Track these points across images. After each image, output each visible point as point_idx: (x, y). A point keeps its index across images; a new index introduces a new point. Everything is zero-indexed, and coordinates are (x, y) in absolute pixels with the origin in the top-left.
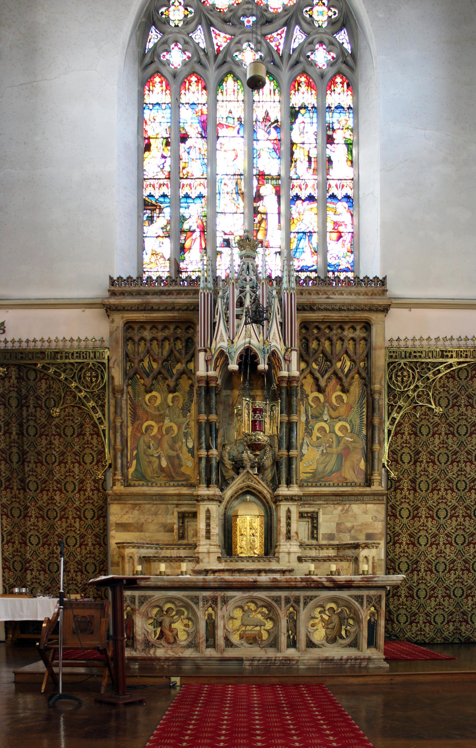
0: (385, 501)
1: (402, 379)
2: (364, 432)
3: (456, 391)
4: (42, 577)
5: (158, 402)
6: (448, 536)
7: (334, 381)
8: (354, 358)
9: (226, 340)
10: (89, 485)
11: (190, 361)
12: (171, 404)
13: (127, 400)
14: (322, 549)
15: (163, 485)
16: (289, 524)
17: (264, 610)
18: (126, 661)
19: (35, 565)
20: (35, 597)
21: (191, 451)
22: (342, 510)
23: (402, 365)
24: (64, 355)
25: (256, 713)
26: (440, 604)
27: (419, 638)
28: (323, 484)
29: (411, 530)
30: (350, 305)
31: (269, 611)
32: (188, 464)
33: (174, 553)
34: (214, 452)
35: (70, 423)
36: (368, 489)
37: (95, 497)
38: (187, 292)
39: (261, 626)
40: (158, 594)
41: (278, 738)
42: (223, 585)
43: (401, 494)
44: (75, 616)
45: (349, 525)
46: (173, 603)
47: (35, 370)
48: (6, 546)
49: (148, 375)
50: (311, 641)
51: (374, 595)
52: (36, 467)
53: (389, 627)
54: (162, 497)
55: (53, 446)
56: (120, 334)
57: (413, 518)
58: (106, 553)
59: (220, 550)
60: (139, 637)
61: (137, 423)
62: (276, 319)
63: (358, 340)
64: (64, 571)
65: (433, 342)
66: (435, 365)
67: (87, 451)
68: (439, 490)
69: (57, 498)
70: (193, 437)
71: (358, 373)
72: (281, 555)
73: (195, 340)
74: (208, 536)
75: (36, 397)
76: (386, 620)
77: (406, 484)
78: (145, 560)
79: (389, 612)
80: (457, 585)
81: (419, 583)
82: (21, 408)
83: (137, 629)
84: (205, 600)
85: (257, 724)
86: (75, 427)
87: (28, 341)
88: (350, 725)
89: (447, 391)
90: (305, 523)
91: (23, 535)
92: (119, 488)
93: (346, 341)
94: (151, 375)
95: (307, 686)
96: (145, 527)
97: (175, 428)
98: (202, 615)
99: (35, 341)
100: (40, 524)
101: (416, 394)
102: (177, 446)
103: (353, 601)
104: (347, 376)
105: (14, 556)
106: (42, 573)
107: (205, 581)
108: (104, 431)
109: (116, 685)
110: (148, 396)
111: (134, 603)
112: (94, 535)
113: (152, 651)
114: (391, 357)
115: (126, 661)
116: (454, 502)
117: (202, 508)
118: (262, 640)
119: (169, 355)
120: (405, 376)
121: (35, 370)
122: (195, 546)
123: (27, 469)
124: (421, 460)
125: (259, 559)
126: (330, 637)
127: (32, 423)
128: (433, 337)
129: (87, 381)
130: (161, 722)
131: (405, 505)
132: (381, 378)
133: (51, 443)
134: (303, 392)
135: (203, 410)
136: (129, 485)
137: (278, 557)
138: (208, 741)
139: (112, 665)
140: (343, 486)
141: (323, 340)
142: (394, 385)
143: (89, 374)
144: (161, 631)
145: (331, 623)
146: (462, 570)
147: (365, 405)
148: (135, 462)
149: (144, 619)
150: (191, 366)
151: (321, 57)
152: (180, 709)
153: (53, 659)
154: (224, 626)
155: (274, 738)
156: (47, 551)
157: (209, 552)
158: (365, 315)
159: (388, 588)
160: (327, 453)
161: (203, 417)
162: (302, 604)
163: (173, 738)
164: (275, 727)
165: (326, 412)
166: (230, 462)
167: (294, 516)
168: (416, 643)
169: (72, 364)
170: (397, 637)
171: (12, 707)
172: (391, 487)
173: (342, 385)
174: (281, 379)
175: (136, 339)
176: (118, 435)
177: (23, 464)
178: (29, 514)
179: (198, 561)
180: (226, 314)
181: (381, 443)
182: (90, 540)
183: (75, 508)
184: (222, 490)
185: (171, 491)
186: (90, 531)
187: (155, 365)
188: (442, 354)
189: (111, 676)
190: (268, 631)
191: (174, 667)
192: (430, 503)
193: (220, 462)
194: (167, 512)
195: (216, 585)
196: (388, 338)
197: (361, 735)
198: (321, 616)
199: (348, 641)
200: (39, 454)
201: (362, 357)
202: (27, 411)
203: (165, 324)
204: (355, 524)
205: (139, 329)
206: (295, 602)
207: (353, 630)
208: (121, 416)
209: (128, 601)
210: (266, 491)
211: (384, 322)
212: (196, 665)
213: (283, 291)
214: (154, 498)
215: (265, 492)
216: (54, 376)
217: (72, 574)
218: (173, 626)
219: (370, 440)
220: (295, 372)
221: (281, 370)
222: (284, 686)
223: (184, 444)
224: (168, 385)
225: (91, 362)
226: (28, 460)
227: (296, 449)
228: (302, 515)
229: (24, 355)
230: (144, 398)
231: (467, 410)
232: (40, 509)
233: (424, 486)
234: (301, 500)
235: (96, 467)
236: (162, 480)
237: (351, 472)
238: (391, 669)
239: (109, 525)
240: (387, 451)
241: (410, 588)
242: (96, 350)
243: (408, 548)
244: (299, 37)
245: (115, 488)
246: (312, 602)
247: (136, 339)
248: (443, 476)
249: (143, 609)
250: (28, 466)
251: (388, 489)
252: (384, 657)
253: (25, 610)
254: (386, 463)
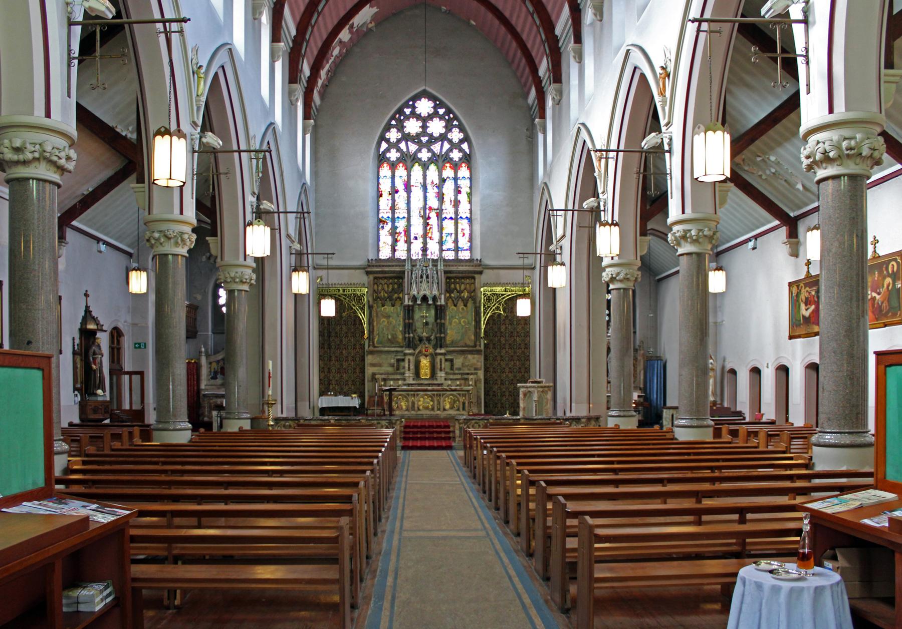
10: (358, 346)
74: (409, 370)
122: (404, 374)
150: (401, 295)
151: (456, 155)
157: (409, 375)
179: (405, 380)
182: (358, 370)
185: (393, 349)
203: (391, 278)
228: (446, 360)
244: (446, 146)
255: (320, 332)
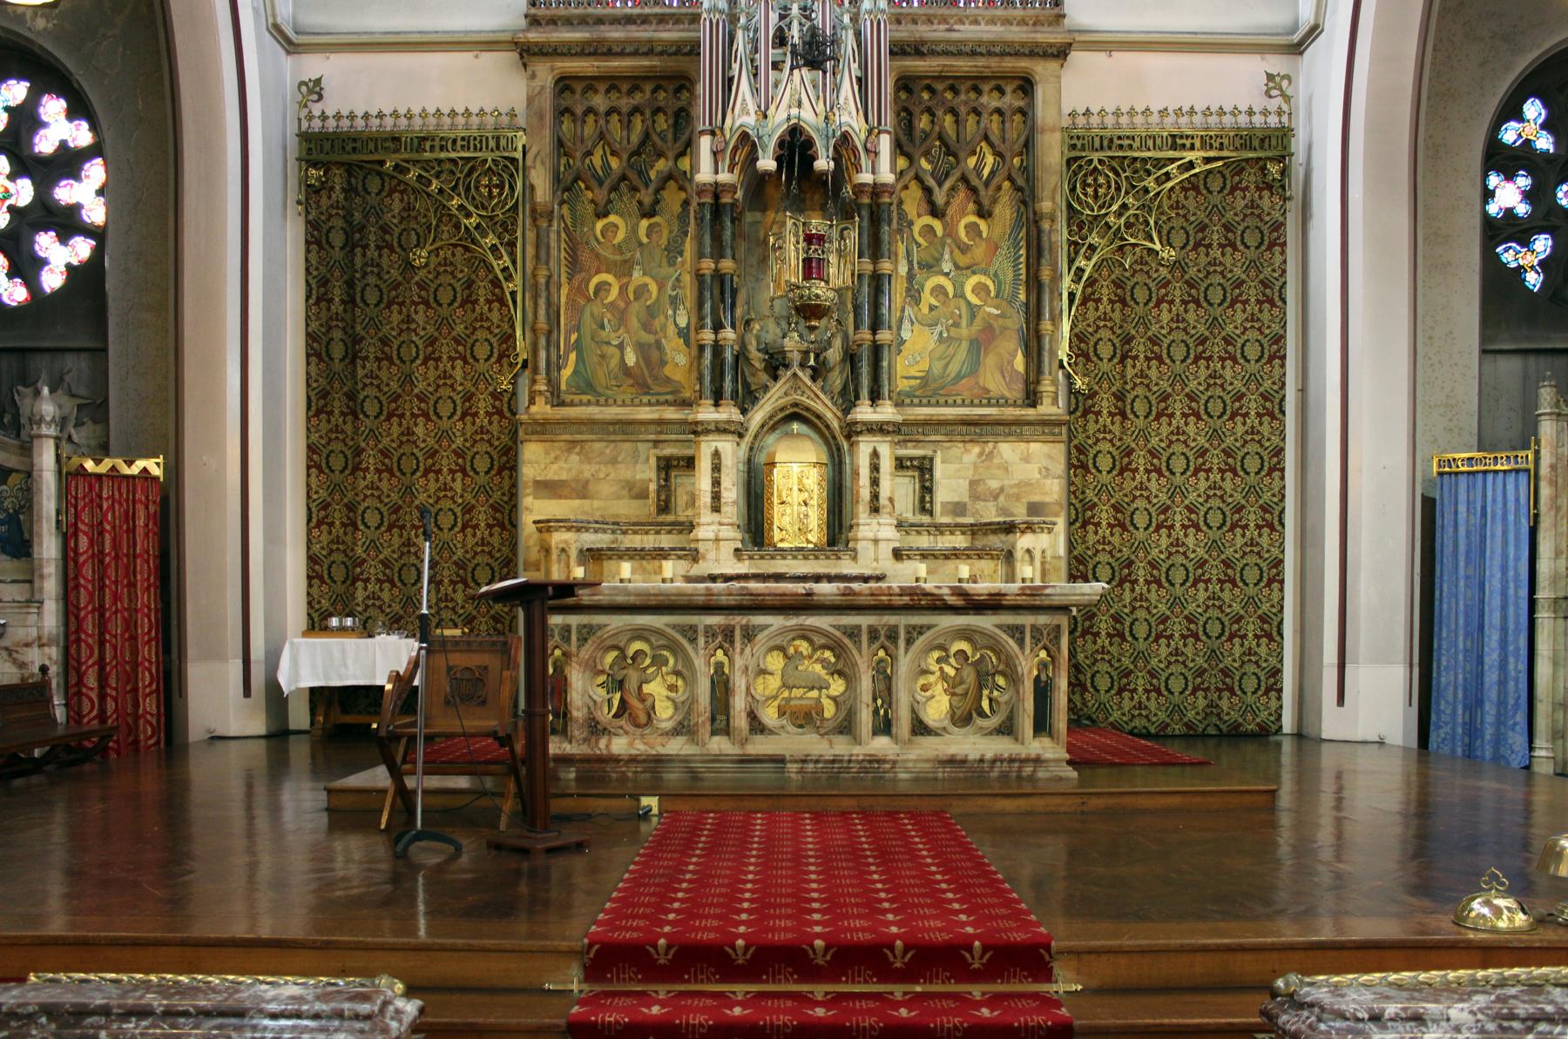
0: (1064, 437)
1: (1096, 191)
2: (1022, 297)
3: (1202, 215)
4: (386, 596)
5: (621, 235)
6: (1191, 511)
7: (962, 194)
8: (1002, 148)
9: (752, 112)
10: (483, 404)
11: (682, 154)
12: (645, 240)
13: (559, 233)
14: (942, 533)
15: (628, 401)
16: (875, 482)
17: (828, 654)
18: (552, 765)
19: (373, 569)
20: (371, 636)
21: (684, 334)
22: (981, 454)
23: (1096, 162)
24: (437, 143)
25: (812, 868)
26: (1177, 652)
27: (1137, 723)
28: (942, 401)
29: (1118, 496)
30: (993, 43)
31: (837, 657)
32: (678, 358)
33: (649, 541)
34: (729, 334)
35: (448, 279)
36: (1031, 411)
37: (495, 428)
38: (676, 19)
39: (820, 689)
40: (616, 622)
41: (854, 917)
42: (746, 600)
43: (1097, 422)
44: (450, 669)
45: (994, 484)
46: (647, 640)
47: (380, 174)
48: (316, 532)
49: (601, 183)
50: (921, 722)
51: (1046, 626)
52: (380, 368)
53: (1077, 698)
54: (626, 428)
55: (413, 326)
56: (547, 101)
57: (1121, 473)
58: (514, 546)
59: (739, 535)
60: (578, 713)
61: (579, 277)
62: (850, 70)
63: (1008, 114)
64: (430, 582)
65: (1155, 119)
66: (1159, 163)
67: (480, 334)
68: (1172, 415)
69: (419, 430)
70: (688, 305)
71: (1010, 178)
72: (860, 546)
73: (693, 114)
75: (381, 228)
76: (1070, 683)
77: (1105, 403)
78: (592, 556)
79: (1075, 668)
80: (1211, 613)
81: (1134, 608)
82: (352, 250)
83: (574, 695)
84: (710, 632)
85: (814, 890)
86: (458, 286)
87: (366, 116)
88: (1000, 893)
89: (1184, 216)
90: (907, 480)
91: (351, 507)
92: (541, 409)
93: (985, 115)
94: (607, 183)
95: (912, 815)
96: (592, 488)
97: (653, 288)
98: (703, 663)
99: (380, 115)
100: (384, 485)
101: (1122, 220)
102: (657, 324)
103: (1004, 636)
104: (987, 184)
105: (332, 551)
106: (386, 585)
107: (709, 593)
108: (513, 294)
109: (532, 811)
110: (600, 225)
111: (567, 639)
112: (491, 506)
113: (603, 743)
114: (1074, 147)
115: (552, 765)
116: (1202, 441)
117: (705, 450)
118: (823, 719)
119: (643, 143)
120: (1100, 186)
121: (380, 174)
122: (691, 526)
123: (360, 372)
124: (1134, 353)
125: (815, 552)
126: (958, 712)
127: (372, 280)
128: (1155, 108)
129: (481, 195)
130: (621, 885)
131: (1105, 446)
132: (1054, 190)
133: (409, 320)
134: (902, 215)
135: (708, 250)
136: (562, 404)
137: (854, 550)
138: (715, 923)
139: (523, 771)
140: (981, 405)
141: (940, 113)
142: (1080, 204)
143: (485, 181)
144: (622, 700)
145: (962, 683)
146: (1219, 581)
147: (1023, 243)
148: (573, 356)
149: (588, 674)
150: (685, 164)
152: (659, 859)
153: (404, 761)
154: (748, 689)
155: (847, 916)
156: (396, 541)
158: (1023, 64)
159: (1074, 610)
160: (949, 337)
161: (708, 265)
162: (902, 643)
163: (644, 916)
164: (853, 906)
165: (947, 256)
166: (760, 355)
167: (886, 464)
168: (1131, 733)
169: (452, 161)
170: (1094, 721)
171: (321, 859)
172: (1076, 409)
173: (978, 203)
174: (859, 189)
175: (579, 110)
176: (542, 302)
177: (353, 362)
178: (364, 465)
179: (694, 556)
180: (752, 61)
181: (1056, 320)
182: (482, 517)
183: (454, 451)
184: (744, 411)
185: (645, 413)
186: (482, 498)
187: (614, 163)
188: (1174, 142)
189: (520, 794)
190: (834, 699)
191: (648, 775)
192: (1154, 441)
193: (741, 356)
194: (635, 457)
195: (732, 601)
196: (1066, 110)
197: (1022, 912)
198: (941, 669)
199: (994, 722)
200: (384, 341)
201: (1017, 147)
202: (364, 255)
203: (635, 82)
204: (1006, 482)
205: (584, 92)
206: (889, 637)
207: (1004, 699)
208: (547, 263)
209: (557, 637)
210: (827, 409)
211: (1059, 77)
212: (692, 771)
213: (864, 16)
214: (611, 428)
215: (829, 415)
216: (417, 185)
217: (446, 588)
218: (647, 688)
219: (1034, 313)
220: (886, 176)
221: (859, 170)
222: (866, 815)
223: (671, 320)
224: (640, 202)
225: (490, 157)
226: (363, 354)
227: (890, 328)
229: (358, 145)
230: (593, 229)
231: (1223, 255)
232: (385, 453)
233: (1140, 407)
234: (898, 432)
235: (496, 367)
236: (628, 393)
237: (998, 377)
238: (1082, 782)
239: (521, 486)
240: (1066, 334)
241: (1117, 618)
242: (501, 133)
243: (1112, 534)
245: (534, 409)
246: (922, 638)
247: (579, 110)
248: (1178, 387)
249: (586, 653)
250: (364, 367)
251: (1070, 413)
252: (1067, 756)
253: (350, 662)
254: (1065, 360)
255: (311, 337)
